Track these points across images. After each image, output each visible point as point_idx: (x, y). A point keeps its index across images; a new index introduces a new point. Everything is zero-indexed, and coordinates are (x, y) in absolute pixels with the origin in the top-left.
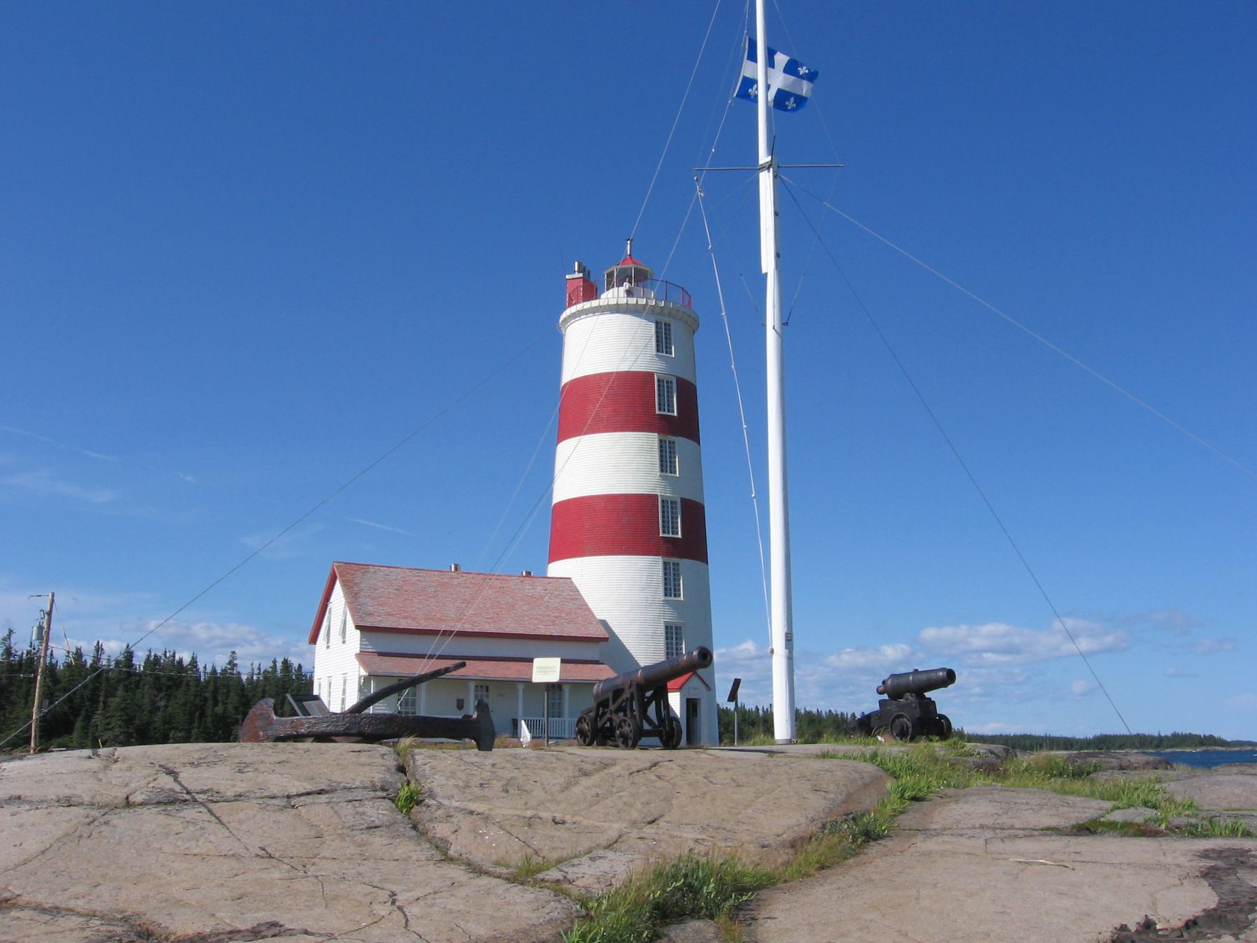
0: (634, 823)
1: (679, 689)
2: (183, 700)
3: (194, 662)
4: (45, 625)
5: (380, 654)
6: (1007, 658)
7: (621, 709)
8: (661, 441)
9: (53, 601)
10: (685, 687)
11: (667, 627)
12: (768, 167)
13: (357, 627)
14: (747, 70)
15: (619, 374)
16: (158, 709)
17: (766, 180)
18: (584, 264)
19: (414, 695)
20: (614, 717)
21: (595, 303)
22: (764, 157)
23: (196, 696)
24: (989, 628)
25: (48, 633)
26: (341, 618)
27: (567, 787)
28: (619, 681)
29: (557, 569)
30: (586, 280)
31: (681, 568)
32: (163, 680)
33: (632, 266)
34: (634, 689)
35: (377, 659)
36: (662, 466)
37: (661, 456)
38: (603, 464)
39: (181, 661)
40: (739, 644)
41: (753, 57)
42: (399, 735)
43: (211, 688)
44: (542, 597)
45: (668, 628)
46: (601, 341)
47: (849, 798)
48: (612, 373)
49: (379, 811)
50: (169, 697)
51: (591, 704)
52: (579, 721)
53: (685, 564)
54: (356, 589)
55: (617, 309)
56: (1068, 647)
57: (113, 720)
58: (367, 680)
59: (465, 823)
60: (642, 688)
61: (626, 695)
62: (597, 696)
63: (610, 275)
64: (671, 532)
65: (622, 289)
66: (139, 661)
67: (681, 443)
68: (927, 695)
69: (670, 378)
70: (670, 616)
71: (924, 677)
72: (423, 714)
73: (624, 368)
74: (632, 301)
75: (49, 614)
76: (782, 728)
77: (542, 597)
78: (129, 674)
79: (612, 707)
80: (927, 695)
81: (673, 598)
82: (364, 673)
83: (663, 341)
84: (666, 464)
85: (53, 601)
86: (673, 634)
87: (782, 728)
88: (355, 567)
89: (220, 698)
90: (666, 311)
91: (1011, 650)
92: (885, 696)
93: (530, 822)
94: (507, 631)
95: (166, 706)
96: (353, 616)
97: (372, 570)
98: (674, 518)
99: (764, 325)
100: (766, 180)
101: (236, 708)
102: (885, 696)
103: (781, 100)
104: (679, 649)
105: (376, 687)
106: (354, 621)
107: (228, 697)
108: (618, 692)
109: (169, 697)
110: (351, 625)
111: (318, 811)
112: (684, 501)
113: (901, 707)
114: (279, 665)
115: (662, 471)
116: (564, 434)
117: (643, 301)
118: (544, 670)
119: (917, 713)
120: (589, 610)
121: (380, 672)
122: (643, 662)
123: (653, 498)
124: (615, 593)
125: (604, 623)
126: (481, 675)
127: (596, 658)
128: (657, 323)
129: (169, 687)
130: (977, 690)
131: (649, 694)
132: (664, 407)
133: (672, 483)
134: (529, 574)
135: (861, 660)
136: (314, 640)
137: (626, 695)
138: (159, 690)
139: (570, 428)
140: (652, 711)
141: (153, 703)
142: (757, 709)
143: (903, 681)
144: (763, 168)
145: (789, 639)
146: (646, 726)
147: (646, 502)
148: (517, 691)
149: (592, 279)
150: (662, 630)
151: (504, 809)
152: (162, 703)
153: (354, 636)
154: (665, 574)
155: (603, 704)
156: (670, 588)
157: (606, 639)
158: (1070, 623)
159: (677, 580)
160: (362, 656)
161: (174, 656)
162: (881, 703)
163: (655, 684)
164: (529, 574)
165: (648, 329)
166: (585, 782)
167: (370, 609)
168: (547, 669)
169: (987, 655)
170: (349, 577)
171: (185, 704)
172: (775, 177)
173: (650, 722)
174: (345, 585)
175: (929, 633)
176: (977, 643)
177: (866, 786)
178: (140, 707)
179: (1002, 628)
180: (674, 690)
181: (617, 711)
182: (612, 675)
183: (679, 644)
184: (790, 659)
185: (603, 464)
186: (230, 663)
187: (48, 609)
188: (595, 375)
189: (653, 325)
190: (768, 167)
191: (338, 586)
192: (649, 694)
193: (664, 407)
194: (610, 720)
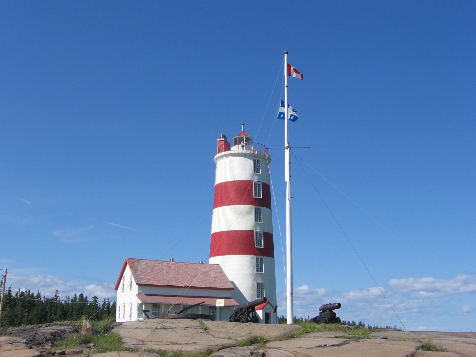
0: (247, 333)
1: (262, 309)
2: (36, 313)
3: (39, 296)
4: (3, 281)
5: (146, 295)
6: (430, 294)
7: (242, 314)
8: (255, 209)
9: (7, 271)
10: (265, 308)
11: (257, 284)
12: (288, 148)
13: (137, 284)
14: (281, 110)
15: (239, 181)
16: (24, 316)
17: (287, 152)
18: (224, 134)
19: (159, 310)
20: (240, 316)
21: (229, 152)
22: (286, 145)
23: (42, 311)
24: (426, 279)
25: (5, 285)
26: (129, 280)
27: (234, 327)
28: (242, 306)
29: (214, 260)
30: (225, 142)
31: (263, 260)
32: (26, 303)
33: (244, 136)
34: (246, 309)
35: (145, 296)
36: (256, 219)
37: (256, 215)
38: (231, 218)
39: (33, 294)
40: (301, 286)
41: (283, 105)
42: (198, 318)
43: (48, 306)
44: (208, 272)
45: (258, 284)
46: (231, 168)
47: (291, 331)
48: (236, 181)
49: (201, 330)
50: (30, 311)
51: (234, 313)
52: (230, 317)
53: (265, 258)
54: (136, 269)
55: (238, 155)
56: (463, 289)
57: (5, 321)
58: (141, 305)
59: (217, 333)
60: (248, 308)
61: (244, 310)
62: (235, 310)
63: (235, 140)
64: (260, 246)
65: (240, 145)
66: (14, 295)
67: (264, 209)
68: (334, 311)
69: (259, 183)
70: (258, 280)
71: (332, 306)
72: (200, 313)
73: (241, 179)
74: (244, 152)
75: (5, 277)
76: (289, 321)
77: (208, 272)
78: (10, 300)
79: (240, 314)
80: (334, 311)
81: (260, 272)
82: (140, 302)
83: (256, 168)
84: (257, 218)
85: (7, 271)
86: (260, 287)
87: (289, 321)
88: (134, 260)
89: (52, 312)
90: (258, 155)
91: (435, 290)
92: (321, 311)
93: (228, 333)
94: (194, 286)
95: (28, 315)
96: (135, 280)
97: (141, 261)
98: (261, 240)
99: (286, 198)
100: (287, 152)
101: (60, 316)
102: (321, 311)
103: (294, 119)
104: (262, 293)
105: (145, 307)
106: (136, 282)
107: (56, 311)
108: (241, 309)
109: (30, 311)
110: (134, 284)
111: (190, 330)
112: (264, 232)
113: (325, 315)
114: (78, 296)
115: (256, 221)
116: (216, 205)
117: (248, 152)
118: (219, 303)
119: (330, 316)
120: (226, 277)
121: (147, 302)
122: (250, 301)
123: (252, 232)
124: (237, 269)
125: (232, 282)
126: (185, 303)
127: (229, 297)
128: (254, 160)
129: (29, 306)
130: (415, 310)
131: (250, 310)
132: (258, 195)
133: (260, 225)
134: (202, 262)
135: (359, 295)
136: (117, 288)
137: (244, 310)
138: (25, 308)
139: (218, 204)
140: (251, 315)
141: (23, 314)
142: (302, 318)
143: (326, 307)
144: (286, 148)
145: (292, 294)
146: (249, 319)
147: (250, 233)
148: (199, 309)
149: (228, 140)
150: (255, 285)
151: (223, 330)
152: (26, 314)
153: (136, 288)
154: (257, 262)
155: (237, 313)
156: (259, 268)
157: (233, 289)
158: (464, 277)
159: (261, 265)
160: (139, 295)
161: (29, 291)
162: (320, 313)
163: (252, 307)
164: (202, 262)
165: (251, 163)
166: (237, 327)
167: (141, 277)
168: (220, 303)
169: (422, 293)
170: (132, 264)
171: (37, 314)
172: (290, 151)
173: (250, 318)
174: (132, 267)
175: (394, 282)
176: (417, 286)
177: (296, 330)
178: (16, 315)
179: (429, 279)
180: (259, 309)
181: (241, 315)
182: (236, 304)
183: (262, 291)
184: (292, 300)
185: (231, 218)
186: (55, 295)
187: (5, 275)
188: (229, 182)
189: (253, 161)
190: (288, 148)
191: (128, 267)
192: (250, 310)
193: (258, 195)
194: (239, 317)
